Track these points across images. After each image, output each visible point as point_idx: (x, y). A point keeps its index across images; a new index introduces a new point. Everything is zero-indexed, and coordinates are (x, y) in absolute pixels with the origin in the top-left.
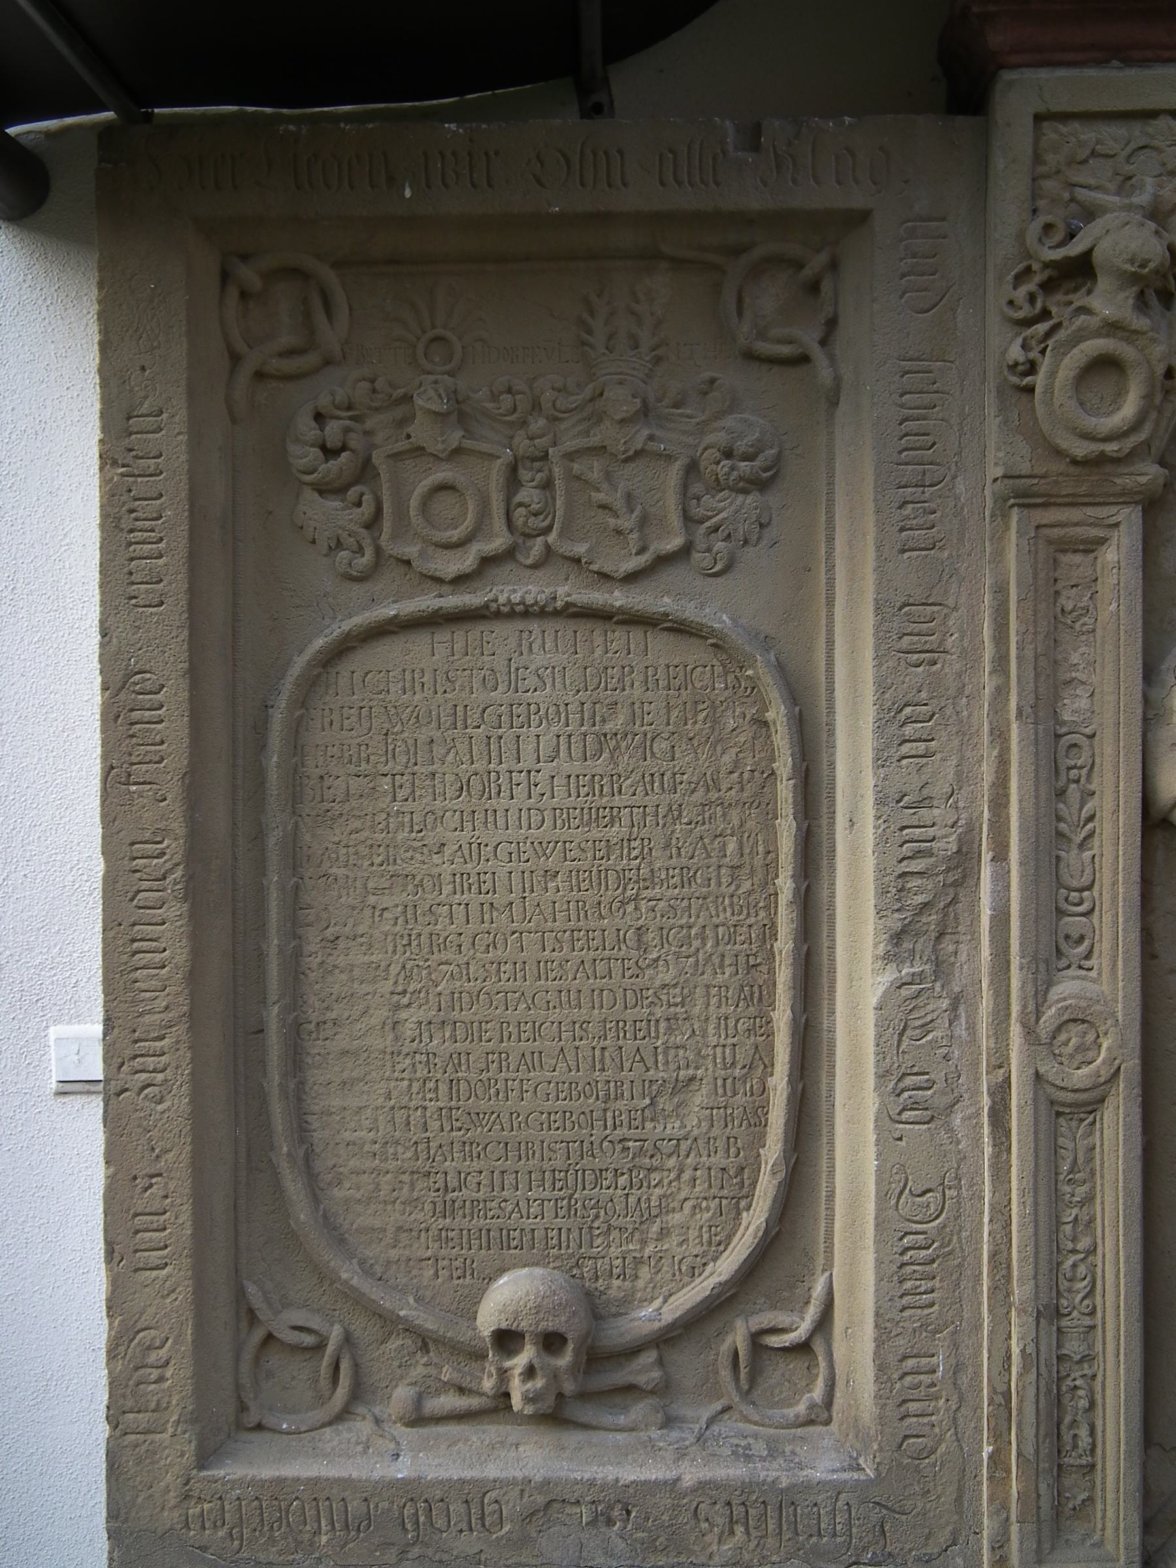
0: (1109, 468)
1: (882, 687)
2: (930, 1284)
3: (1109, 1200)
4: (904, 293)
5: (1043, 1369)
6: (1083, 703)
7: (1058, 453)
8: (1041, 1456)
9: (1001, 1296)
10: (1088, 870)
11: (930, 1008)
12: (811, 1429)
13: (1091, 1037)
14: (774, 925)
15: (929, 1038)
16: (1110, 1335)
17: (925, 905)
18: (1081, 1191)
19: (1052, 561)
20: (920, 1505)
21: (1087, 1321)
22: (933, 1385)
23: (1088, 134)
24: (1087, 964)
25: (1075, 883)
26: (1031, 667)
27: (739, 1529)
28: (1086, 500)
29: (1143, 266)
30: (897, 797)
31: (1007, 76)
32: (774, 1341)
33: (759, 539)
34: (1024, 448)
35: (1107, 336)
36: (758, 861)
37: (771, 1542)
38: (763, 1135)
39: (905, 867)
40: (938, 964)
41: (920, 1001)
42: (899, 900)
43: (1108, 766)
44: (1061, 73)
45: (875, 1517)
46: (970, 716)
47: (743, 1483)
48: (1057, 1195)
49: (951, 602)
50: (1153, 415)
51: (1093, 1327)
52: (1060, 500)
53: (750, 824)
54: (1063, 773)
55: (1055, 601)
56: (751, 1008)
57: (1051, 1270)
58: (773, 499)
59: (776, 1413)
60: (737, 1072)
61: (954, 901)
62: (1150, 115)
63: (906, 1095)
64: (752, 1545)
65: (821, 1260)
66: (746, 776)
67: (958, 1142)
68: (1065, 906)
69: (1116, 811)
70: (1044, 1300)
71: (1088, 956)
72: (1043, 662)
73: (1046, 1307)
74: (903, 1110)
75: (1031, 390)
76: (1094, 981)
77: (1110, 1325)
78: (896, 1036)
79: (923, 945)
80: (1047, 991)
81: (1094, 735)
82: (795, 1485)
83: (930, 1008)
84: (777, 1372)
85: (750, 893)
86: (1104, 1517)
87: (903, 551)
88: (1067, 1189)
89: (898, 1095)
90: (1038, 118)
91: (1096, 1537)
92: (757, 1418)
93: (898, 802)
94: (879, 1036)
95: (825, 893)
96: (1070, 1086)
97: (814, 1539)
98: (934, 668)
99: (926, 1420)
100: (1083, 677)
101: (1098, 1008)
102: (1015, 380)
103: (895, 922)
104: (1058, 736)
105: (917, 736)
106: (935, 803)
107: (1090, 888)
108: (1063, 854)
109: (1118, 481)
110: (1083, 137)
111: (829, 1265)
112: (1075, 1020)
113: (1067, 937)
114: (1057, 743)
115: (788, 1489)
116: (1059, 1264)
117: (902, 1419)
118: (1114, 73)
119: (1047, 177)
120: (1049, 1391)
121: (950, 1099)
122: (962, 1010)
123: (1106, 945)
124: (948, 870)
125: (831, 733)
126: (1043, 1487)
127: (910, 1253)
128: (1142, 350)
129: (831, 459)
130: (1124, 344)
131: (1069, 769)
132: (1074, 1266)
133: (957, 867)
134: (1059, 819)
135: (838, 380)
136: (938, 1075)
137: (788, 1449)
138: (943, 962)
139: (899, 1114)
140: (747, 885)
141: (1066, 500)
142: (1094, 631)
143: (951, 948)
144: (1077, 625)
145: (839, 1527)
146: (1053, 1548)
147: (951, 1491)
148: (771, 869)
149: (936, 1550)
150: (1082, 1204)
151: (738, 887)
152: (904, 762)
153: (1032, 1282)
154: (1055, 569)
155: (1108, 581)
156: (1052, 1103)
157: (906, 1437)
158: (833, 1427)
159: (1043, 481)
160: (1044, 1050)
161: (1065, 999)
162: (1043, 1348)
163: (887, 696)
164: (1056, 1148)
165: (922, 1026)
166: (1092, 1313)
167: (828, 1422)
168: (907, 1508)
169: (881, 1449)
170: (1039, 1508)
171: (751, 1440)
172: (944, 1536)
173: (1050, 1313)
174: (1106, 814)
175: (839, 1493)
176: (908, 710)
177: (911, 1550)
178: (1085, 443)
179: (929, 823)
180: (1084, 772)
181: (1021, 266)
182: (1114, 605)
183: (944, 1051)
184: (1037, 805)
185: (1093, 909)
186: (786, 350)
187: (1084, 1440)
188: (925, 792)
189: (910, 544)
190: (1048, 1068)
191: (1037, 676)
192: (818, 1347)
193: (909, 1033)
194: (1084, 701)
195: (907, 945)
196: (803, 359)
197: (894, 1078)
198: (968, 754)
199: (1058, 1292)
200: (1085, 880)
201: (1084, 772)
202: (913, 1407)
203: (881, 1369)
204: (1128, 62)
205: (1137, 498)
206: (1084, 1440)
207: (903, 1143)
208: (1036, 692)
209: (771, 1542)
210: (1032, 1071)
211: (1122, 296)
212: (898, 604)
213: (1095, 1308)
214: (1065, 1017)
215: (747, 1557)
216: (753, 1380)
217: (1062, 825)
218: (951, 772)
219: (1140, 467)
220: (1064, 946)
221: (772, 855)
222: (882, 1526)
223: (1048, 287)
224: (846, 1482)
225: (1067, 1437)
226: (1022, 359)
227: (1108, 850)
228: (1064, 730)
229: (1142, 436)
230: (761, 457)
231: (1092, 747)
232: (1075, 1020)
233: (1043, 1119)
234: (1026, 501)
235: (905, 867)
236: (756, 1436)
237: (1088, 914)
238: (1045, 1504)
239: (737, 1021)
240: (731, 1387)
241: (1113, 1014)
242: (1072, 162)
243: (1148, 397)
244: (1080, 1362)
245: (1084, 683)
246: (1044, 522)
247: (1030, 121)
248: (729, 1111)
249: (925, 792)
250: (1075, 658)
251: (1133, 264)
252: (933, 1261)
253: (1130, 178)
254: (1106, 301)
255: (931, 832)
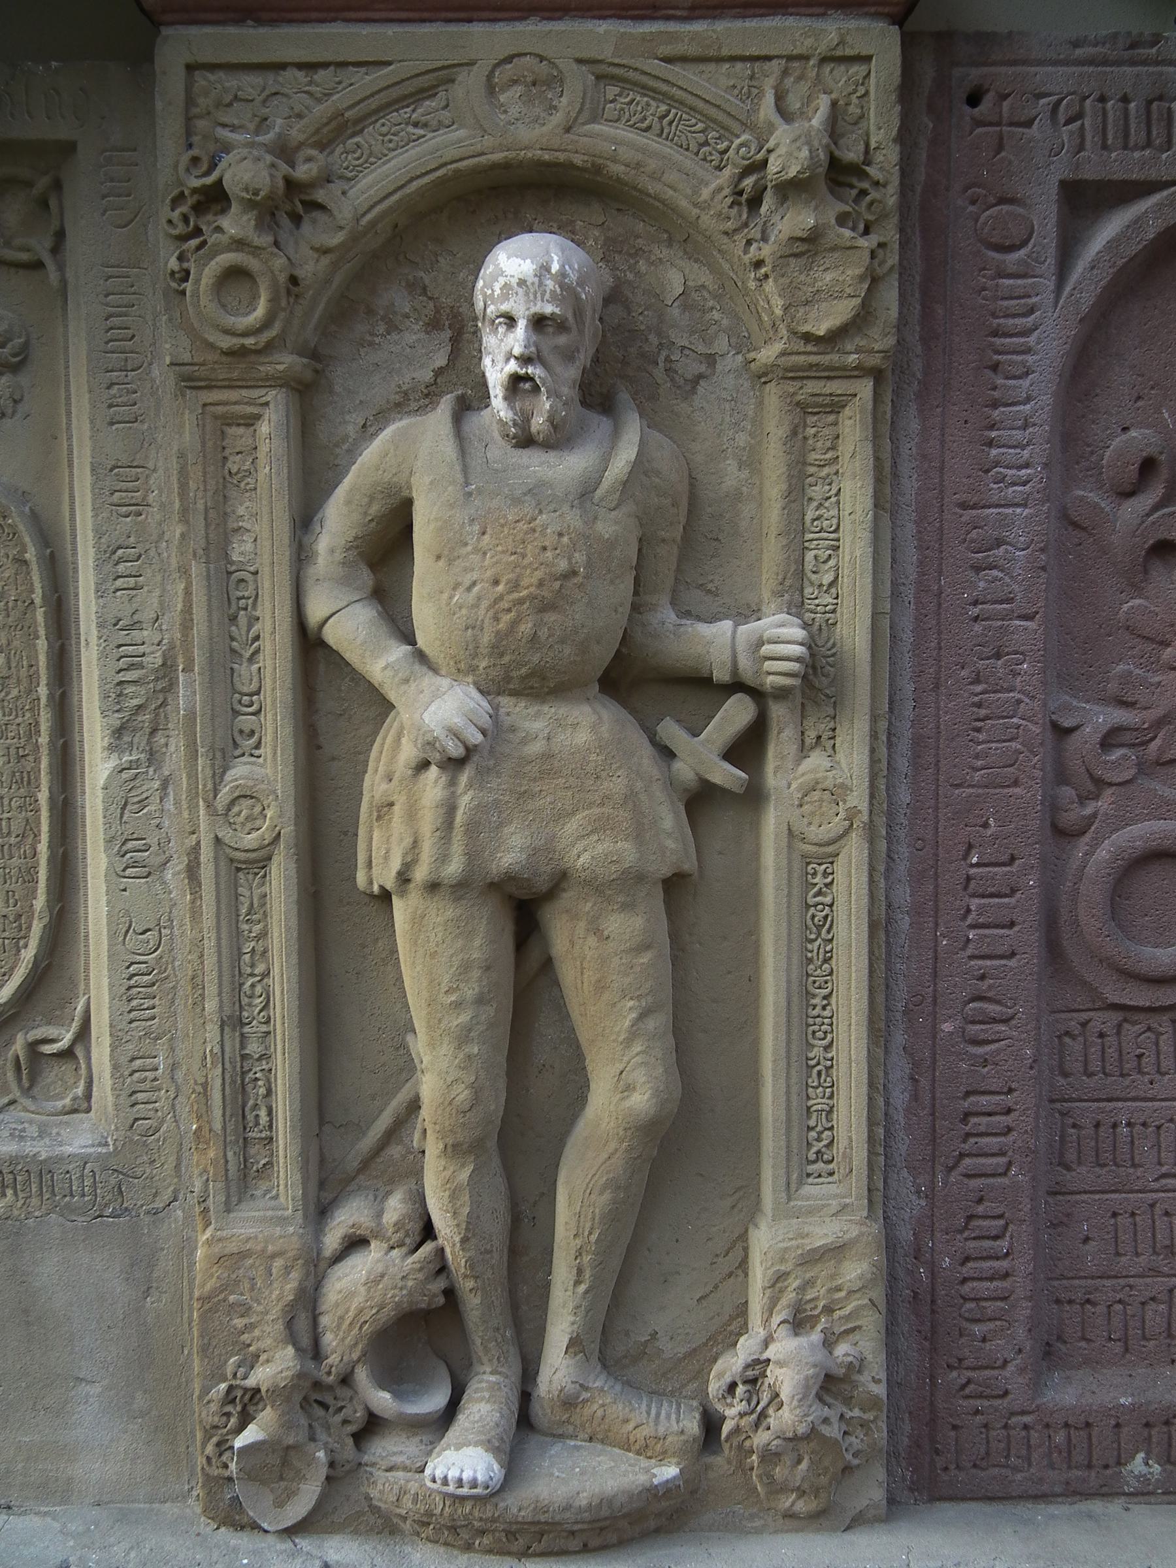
0: (253, 358)
1: (99, 534)
2: (152, 1002)
3: (276, 935)
4: (105, 211)
5: (227, 1065)
6: (249, 547)
7: (212, 346)
8: (228, 1131)
9: (198, 1010)
10: (255, 679)
11: (145, 788)
12: (75, 1116)
13: (258, 809)
14: (37, 723)
15: (145, 811)
16: (279, 1037)
17: (140, 707)
18: (257, 928)
19: (219, 433)
20: (148, 1171)
21: (264, 1028)
22: (155, 1079)
23: (232, 82)
24: (257, 753)
25: (245, 689)
26: (202, 518)
27: (9, 1192)
28: (239, 383)
29: (256, 193)
30: (114, 621)
31: (166, 31)
32: (48, 1049)
33: (14, 413)
34: (185, 341)
35: (237, 250)
36: (23, 672)
37: (35, 1201)
38: (35, 890)
39: (122, 677)
40: (152, 753)
41: (137, 782)
42: (118, 703)
43: (267, 597)
44: (208, 30)
45: (113, 1181)
46: (169, 556)
47: (11, 1156)
48: (239, 933)
49: (151, 465)
50: (282, 315)
51: (269, 1033)
52: (219, 383)
53: (16, 643)
54: (234, 602)
55: (224, 465)
56: (22, 790)
57: (233, 990)
58: (23, 379)
59: (50, 1106)
60: (13, 840)
61: (164, 704)
62: (282, 66)
63: (128, 855)
64: (19, 1204)
65: (82, 987)
66: (10, 604)
67: (170, 893)
68: (238, 707)
69: (273, 633)
70: (227, 1011)
71: (258, 746)
72: (212, 514)
73: (229, 1017)
74: (127, 867)
75: (183, 293)
76: (262, 766)
77: (278, 1032)
78: (119, 811)
79: (140, 739)
80: (224, 773)
81: (257, 573)
82: (51, 1158)
83: (145, 788)
84: (52, 1074)
85: (18, 698)
86: (278, 1177)
87: (112, 424)
88: (246, 927)
89: (123, 856)
90: (190, 68)
91: (274, 1192)
92: (33, 1108)
93: (115, 625)
94: (106, 810)
95: (76, 698)
96: (241, 847)
97: (67, 1199)
98: (140, 518)
99: (151, 1106)
100: (248, 527)
101: (263, 786)
102: (174, 285)
103: (115, 720)
104: (229, 573)
105: (128, 573)
106: (144, 626)
107: (258, 693)
108: (236, 666)
109: (261, 369)
110: (227, 84)
111: (87, 990)
112: (245, 796)
113: (241, 732)
114: (228, 579)
115: (45, 1160)
116: (241, 985)
117: (132, 1106)
118: (251, 31)
119: (200, 117)
120: (234, 1082)
121: (162, 858)
122: (170, 790)
123: (269, 738)
124: (157, 679)
125: (76, 570)
126: (230, 1154)
127: (136, 978)
128: (266, 262)
129: (66, 348)
130: (250, 257)
131: (239, 599)
132: (253, 986)
133: (164, 677)
134: (233, 639)
135: (64, 282)
136: (153, 841)
137: (54, 1131)
138: (157, 752)
139: (124, 870)
140: (15, 693)
141: (224, 383)
142: (255, 489)
143: (163, 741)
144: (242, 485)
145: (86, 1189)
146: (240, 1201)
147: (172, 1159)
148: (33, 678)
149: (161, 1205)
150: (258, 938)
151: (8, 694)
152: (119, 593)
153: (217, 999)
154: (223, 439)
155: (264, 449)
156: (232, 860)
157: (136, 1120)
158: (92, 1114)
159: (202, 368)
160: (221, 820)
161: (236, 780)
162: (227, 1049)
163: (103, 540)
164: (237, 896)
165: (139, 802)
166: (268, 1022)
167: (88, 1110)
168: (139, 1174)
169: (117, 1129)
170: (227, 1170)
171: (26, 1125)
172: (167, 1195)
173: (234, 1022)
174: (266, 636)
175: (86, 1163)
176: (120, 552)
177: (142, 1206)
178: (228, 338)
179: (139, 642)
180: (250, 601)
181: (175, 192)
182: (268, 468)
183: (157, 821)
184: (210, 627)
185: (260, 710)
186: (24, 257)
187: (264, 1119)
188: (136, 617)
189: (117, 418)
190: (225, 834)
191: (207, 526)
192: (79, 1051)
193: (129, 807)
194: (249, 545)
195: (127, 739)
196: (39, 265)
197: (119, 843)
198: (169, 587)
199: (241, 1006)
200: (254, 687)
201: (250, 601)
202: (140, 1096)
203: (115, 1067)
204: (260, 22)
205: (279, 382)
206: (264, 1119)
207: (127, 893)
208: (207, 537)
209: (35, 1201)
210: (212, 836)
211: (245, 218)
212: (109, 467)
213: (269, 1017)
214: (236, 794)
215: (16, 1213)
216: (33, 1081)
217: (234, 643)
218: (156, 601)
219: (277, 357)
220: (238, 739)
221: (34, 668)
222: (120, 1188)
223: (199, 209)
224: (90, 1154)
225: (250, 1117)
226: (177, 268)
227: (269, 662)
228: (234, 568)
229: (273, 333)
230: (9, 346)
231: (256, 581)
232: (245, 796)
233: (223, 873)
234: (192, 384)
235: (122, 677)
236: (31, 1122)
237: (257, 713)
238: (232, 1168)
239: (11, 800)
240: (14, 1085)
241: (274, 792)
242: (219, 104)
243: (274, 300)
244: (260, 1059)
245: (249, 531)
246: (209, 401)
247: (182, 72)
248: (7, 871)
249: (136, 617)
250: (241, 511)
251: (248, 192)
252: (154, 984)
253: (266, 119)
254: (234, 223)
255: (141, 649)
